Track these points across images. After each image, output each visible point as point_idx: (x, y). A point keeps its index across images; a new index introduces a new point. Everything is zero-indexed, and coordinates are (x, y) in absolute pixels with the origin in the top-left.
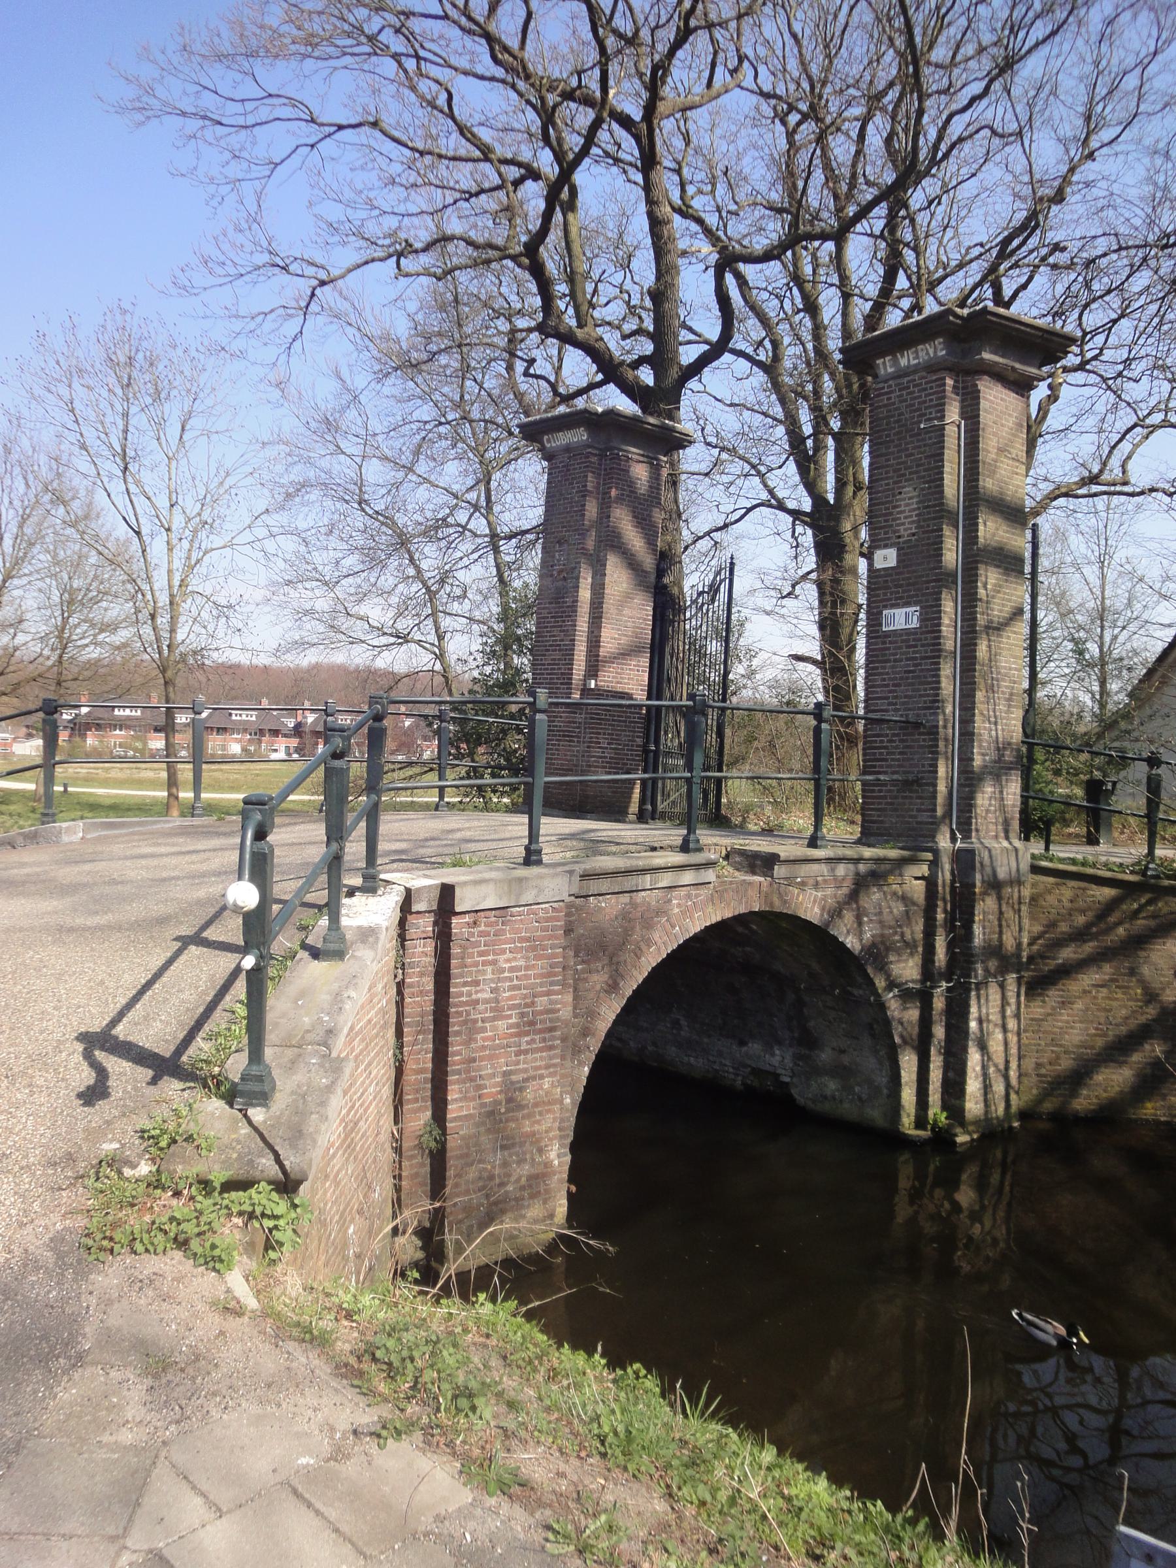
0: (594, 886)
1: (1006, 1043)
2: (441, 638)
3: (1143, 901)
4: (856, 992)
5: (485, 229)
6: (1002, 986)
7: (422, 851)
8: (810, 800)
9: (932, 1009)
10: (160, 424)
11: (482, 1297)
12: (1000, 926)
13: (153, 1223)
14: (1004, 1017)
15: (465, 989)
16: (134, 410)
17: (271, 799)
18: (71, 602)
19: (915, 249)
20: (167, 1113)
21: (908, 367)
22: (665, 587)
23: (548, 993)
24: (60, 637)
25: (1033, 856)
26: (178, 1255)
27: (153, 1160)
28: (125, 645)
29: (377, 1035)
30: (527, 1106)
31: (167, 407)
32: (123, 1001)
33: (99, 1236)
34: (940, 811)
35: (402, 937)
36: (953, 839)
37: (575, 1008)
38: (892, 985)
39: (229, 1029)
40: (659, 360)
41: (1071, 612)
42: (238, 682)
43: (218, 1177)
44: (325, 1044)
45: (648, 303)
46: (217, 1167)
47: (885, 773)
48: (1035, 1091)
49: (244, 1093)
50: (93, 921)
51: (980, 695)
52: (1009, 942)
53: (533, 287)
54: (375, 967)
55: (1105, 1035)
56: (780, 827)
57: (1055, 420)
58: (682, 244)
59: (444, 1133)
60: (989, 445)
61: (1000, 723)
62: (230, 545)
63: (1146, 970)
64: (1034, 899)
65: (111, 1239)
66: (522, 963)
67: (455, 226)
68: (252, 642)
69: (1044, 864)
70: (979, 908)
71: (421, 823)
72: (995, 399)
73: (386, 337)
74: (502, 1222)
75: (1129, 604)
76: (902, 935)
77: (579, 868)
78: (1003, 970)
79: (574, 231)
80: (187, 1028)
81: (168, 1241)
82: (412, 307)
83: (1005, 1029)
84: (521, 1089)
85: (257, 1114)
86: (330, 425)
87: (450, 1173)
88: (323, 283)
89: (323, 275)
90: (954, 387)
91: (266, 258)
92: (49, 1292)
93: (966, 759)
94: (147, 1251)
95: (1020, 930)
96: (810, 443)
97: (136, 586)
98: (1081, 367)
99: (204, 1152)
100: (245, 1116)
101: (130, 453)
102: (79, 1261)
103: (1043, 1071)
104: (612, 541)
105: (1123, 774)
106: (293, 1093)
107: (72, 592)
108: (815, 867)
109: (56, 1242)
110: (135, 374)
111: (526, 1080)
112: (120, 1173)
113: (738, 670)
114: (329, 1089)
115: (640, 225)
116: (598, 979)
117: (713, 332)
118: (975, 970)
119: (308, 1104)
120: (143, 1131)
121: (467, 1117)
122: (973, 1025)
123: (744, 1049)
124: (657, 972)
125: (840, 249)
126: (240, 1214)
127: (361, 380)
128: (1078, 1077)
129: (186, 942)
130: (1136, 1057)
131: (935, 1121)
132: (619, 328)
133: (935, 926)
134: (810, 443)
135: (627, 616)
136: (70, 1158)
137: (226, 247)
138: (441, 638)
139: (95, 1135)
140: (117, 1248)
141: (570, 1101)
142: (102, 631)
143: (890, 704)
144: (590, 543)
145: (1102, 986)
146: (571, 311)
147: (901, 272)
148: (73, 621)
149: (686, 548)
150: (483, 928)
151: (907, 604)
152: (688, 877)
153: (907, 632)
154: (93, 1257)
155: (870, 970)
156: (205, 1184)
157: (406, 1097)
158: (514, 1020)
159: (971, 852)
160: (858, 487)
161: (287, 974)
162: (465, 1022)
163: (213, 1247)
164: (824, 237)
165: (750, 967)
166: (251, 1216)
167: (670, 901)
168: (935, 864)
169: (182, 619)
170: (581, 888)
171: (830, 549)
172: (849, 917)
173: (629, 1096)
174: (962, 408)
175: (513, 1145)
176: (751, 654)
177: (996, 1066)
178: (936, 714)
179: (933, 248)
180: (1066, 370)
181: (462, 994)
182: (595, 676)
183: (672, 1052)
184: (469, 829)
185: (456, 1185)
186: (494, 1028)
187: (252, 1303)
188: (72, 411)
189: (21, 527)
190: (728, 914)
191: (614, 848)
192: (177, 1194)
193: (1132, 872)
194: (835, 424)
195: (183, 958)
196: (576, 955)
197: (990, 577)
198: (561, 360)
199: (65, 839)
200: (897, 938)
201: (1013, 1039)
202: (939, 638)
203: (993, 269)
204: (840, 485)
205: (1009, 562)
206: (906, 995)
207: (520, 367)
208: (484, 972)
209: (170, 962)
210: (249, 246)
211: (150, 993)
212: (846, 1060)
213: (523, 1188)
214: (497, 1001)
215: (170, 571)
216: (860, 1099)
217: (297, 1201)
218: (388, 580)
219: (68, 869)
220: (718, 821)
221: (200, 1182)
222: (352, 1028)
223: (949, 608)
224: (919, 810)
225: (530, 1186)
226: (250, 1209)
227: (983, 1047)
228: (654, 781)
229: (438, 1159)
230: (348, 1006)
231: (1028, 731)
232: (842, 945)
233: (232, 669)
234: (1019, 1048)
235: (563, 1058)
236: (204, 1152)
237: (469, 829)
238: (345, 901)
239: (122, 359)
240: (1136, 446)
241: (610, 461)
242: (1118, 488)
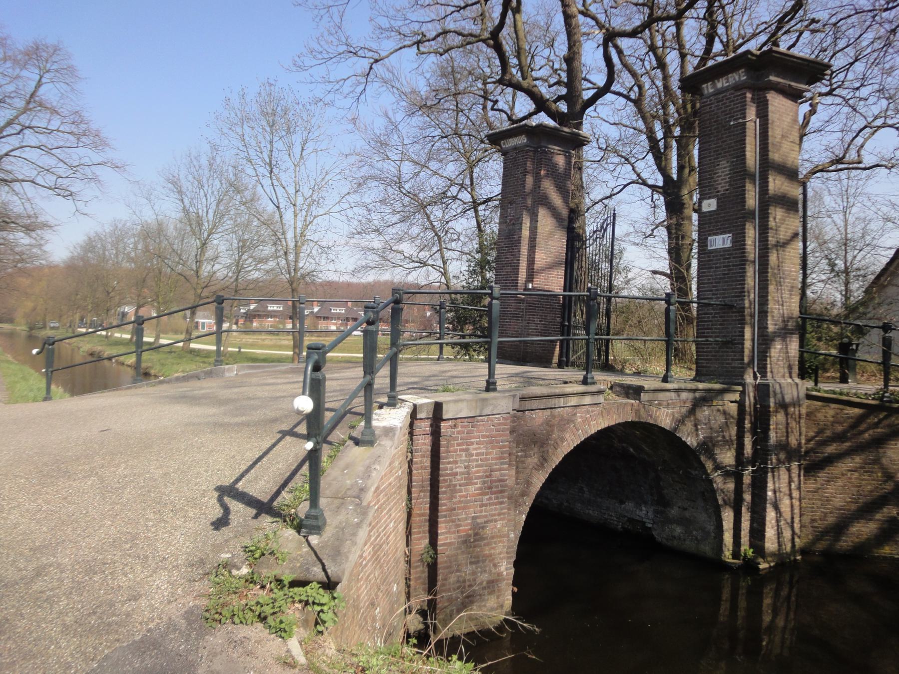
0: (528, 405)
1: (792, 506)
2: (444, 263)
3: (881, 416)
4: (693, 472)
5: (469, 27)
6: (789, 470)
7: (426, 383)
8: (664, 358)
9: (742, 484)
10: (290, 147)
11: (455, 657)
12: (787, 432)
13: (247, 605)
14: (790, 490)
15: (449, 466)
16: (276, 139)
17: (324, 346)
18: (243, 247)
19: (725, 25)
20: (261, 536)
21: (722, 88)
22: (574, 228)
23: (500, 470)
24: (237, 266)
25: (807, 389)
26: (260, 626)
27: (250, 565)
28: (272, 270)
29: (395, 492)
30: (486, 538)
31: (294, 136)
32: (244, 468)
33: (213, 611)
34: (746, 360)
35: (411, 434)
36: (755, 378)
37: (517, 479)
38: (718, 467)
39: (303, 486)
40: (571, 97)
41: (825, 242)
42: (333, 292)
43: (287, 578)
44: (358, 497)
45: (564, 66)
46: (287, 571)
47: (711, 337)
48: (810, 537)
49: (305, 526)
50: (237, 420)
51: (771, 288)
52: (793, 441)
53: (498, 62)
54: (394, 451)
55: (857, 503)
56: (646, 371)
57: (815, 122)
58: (584, 30)
59: (436, 553)
60: (775, 133)
61: (784, 305)
62: (328, 213)
63: (884, 461)
64: (809, 415)
65: (221, 614)
66: (484, 451)
67: (452, 26)
68: (341, 267)
69: (814, 393)
70: (773, 420)
71: (428, 367)
72: (777, 103)
73: (414, 92)
74: (471, 610)
75: (863, 237)
76: (724, 437)
77: (519, 394)
78: (789, 459)
79: (519, 24)
80: (279, 485)
81: (254, 617)
82: (428, 75)
83: (791, 498)
84: (483, 528)
85: (314, 540)
86: (382, 145)
87: (440, 577)
88: (376, 61)
89: (377, 57)
90: (752, 99)
91: (344, 48)
92: (180, 646)
93: (763, 327)
94: (241, 622)
95: (800, 435)
96: (661, 144)
97: (277, 238)
98: (829, 93)
99: (280, 562)
100: (307, 540)
101: (274, 163)
102: (200, 628)
103: (816, 524)
104: (543, 201)
105: (861, 340)
106: (336, 527)
107: (244, 241)
108: (668, 394)
109: (189, 615)
110: (277, 118)
111: (486, 522)
112: (230, 572)
113: (618, 281)
114: (359, 525)
115: (559, 19)
116: (533, 460)
117: (600, 80)
118: (771, 460)
119: (346, 533)
120: (246, 547)
121: (450, 544)
122: (770, 494)
123: (623, 506)
124: (567, 457)
125: (678, 26)
126: (300, 601)
127: (399, 116)
128: (839, 528)
129: (284, 434)
130: (878, 516)
131: (745, 554)
132: (546, 81)
133: (744, 432)
134: (661, 144)
135: (551, 244)
136: (202, 562)
137: (322, 43)
138: (444, 263)
139: (218, 548)
140: (223, 620)
141: (514, 536)
142: (260, 262)
143: (714, 294)
144: (529, 202)
145: (855, 471)
146: (519, 74)
147: (717, 39)
148: (245, 257)
149: (588, 209)
150: (460, 429)
151: (725, 233)
152: (588, 400)
153: (724, 250)
154: (209, 624)
155: (703, 458)
156: (279, 581)
157: (413, 530)
158: (479, 486)
159: (768, 385)
160: (692, 169)
161: (339, 454)
162: (449, 486)
163: (281, 622)
164: (668, 18)
165: (624, 457)
166: (307, 603)
167: (575, 414)
168: (743, 393)
169: (302, 255)
170: (520, 406)
171: (675, 206)
172: (689, 425)
173: (547, 533)
174: (757, 111)
175: (478, 562)
176: (627, 269)
177: (785, 520)
178: (743, 300)
179: (736, 25)
180: (821, 95)
181: (446, 469)
182: (532, 281)
183: (579, 506)
184: (455, 370)
185: (443, 585)
186: (466, 490)
187: (302, 660)
188: (244, 140)
189: (218, 206)
190: (612, 423)
191: (541, 382)
192: (263, 587)
193: (873, 399)
194: (677, 131)
195: (281, 443)
196: (517, 446)
197: (777, 214)
198: (514, 102)
199: (227, 375)
200: (720, 439)
201: (796, 503)
202: (744, 252)
203: (774, 34)
204: (681, 168)
205: (789, 204)
206: (727, 474)
207: (490, 104)
208: (461, 456)
209: (274, 445)
210: (336, 42)
211: (260, 463)
212: (687, 514)
213: (484, 588)
214: (469, 474)
215: (295, 228)
216: (696, 539)
217: (335, 595)
218: (415, 230)
219: (225, 391)
220: (607, 367)
221: (277, 580)
222: (378, 488)
223: (751, 234)
224: (732, 360)
225: (489, 587)
226: (306, 599)
227: (776, 508)
228: (568, 341)
229: (433, 569)
230: (374, 474)
231: (803, 311)
232: (684, 443)
233: (330, 284)
234: (800, 509)
235: (509, 509)
236: (280, 562)
237: (455, 370)
238: (377, 411)
239: (270, 111)
240: (866, 140)
241: (541, 153)
242: (855, 165)
